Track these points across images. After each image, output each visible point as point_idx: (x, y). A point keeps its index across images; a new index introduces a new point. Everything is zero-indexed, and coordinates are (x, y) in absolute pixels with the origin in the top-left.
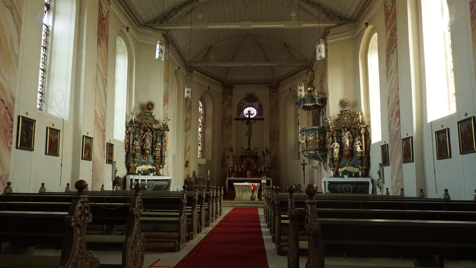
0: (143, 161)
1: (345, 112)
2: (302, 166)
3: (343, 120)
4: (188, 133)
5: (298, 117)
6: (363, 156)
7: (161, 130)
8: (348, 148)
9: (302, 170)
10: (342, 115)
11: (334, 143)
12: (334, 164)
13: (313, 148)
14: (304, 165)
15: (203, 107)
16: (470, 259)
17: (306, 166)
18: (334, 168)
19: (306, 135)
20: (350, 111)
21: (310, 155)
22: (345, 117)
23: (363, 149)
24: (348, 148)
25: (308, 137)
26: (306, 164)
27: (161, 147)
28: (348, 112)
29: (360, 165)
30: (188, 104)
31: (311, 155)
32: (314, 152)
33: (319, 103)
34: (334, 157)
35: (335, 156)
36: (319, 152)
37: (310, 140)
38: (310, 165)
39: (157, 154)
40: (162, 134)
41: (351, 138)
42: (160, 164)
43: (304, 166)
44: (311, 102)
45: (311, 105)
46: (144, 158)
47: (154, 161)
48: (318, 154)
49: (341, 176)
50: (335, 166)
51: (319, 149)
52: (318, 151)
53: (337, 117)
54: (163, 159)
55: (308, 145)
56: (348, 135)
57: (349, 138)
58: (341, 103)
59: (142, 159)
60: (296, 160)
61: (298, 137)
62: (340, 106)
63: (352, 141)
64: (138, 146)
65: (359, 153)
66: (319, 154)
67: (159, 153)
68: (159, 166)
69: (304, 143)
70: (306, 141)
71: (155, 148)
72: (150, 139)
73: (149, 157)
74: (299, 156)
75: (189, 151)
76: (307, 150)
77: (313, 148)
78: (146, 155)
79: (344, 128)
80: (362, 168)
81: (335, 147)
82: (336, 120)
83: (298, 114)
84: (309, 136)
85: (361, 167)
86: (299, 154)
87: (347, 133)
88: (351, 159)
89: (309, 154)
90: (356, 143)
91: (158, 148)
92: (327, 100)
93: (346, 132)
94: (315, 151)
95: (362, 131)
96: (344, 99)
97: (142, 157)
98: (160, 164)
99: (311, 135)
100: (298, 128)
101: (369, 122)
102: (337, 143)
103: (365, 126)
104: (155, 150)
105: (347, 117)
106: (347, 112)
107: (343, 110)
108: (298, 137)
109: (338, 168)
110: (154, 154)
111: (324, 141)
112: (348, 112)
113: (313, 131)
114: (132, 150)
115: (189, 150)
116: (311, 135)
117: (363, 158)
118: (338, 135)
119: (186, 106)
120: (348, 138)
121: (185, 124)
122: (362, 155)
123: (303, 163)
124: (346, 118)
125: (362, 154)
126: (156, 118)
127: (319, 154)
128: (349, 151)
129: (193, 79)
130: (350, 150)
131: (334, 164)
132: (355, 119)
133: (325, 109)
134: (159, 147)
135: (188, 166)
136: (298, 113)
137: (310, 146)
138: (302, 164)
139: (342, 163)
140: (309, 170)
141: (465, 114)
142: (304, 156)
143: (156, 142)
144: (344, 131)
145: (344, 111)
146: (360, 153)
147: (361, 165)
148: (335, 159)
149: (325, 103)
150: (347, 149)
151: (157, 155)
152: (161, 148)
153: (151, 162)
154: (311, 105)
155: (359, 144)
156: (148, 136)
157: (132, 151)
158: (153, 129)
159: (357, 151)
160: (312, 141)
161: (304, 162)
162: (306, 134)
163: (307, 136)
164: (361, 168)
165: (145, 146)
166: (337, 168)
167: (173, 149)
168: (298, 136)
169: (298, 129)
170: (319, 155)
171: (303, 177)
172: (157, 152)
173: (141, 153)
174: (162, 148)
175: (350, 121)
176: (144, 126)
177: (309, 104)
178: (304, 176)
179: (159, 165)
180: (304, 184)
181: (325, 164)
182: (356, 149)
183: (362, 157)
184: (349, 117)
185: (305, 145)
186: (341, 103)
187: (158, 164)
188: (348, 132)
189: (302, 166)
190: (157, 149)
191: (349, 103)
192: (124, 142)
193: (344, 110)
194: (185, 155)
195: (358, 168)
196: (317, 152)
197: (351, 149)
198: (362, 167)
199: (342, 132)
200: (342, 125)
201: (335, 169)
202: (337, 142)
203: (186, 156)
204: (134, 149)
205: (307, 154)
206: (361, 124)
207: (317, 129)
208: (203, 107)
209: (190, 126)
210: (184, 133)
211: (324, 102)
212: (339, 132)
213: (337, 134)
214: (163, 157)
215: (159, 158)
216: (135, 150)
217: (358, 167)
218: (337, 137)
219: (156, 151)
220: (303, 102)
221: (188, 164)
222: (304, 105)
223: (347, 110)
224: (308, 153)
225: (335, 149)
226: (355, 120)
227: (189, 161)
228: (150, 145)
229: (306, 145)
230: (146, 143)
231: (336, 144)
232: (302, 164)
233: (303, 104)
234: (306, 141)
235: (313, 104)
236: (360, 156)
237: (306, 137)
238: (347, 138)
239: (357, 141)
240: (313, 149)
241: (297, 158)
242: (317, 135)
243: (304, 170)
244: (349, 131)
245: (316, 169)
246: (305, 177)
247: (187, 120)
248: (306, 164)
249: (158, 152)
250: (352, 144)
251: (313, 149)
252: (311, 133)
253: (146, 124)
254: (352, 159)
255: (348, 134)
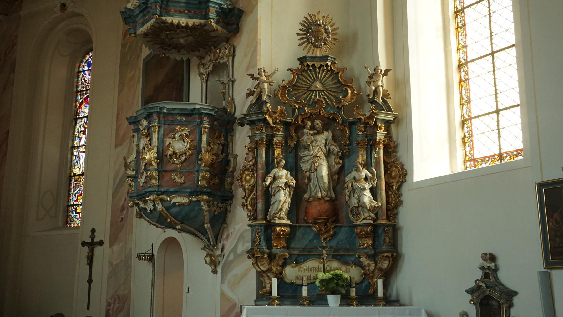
1: (317, 65)
2: (86, 249)
3: (308, 89)
5: (74, 99)
6: (379, 222)
8: (324, 193)
9: (85, 261)
10: (304, 73)
11: (275, 170)
12: (270, 247)
13: (185, 185)
14: (92, 245)
17: (98, 250)
18: (270, 263)
19: (158, 132)
20: (333, 63)
21: (168, 209)
22: (314, 81)
23: (382, 199)
24: (324, 193)
25: (168, 141)
26: (101, 243)
28: (327, 66)
29: (369, 257)
31: (174, 210)
32: (186, 200)
33: (217, 23)
34: (277, 221)
35: (280, 218)
36: (208, 202)
37: (174, 153)
38: (116, 248)
41: (333, 157)
43: (92, 251)
44: (190, 12)
45: (190, 25)
48: (201, 210)
49: (305, 299)
50: (275, 256)
51: (209, 190)
52: (205, 197)
53: (289, 77)
55: (166, 171)
56: (325, 146)
57: (328, 155)
58: (307, 31)
60: (58, 228)
61: (69, 159)
62: (300, 39)
63: (336, 167)
65: (369, 210)
66: (205, 207)
69: (153, 163)
70: (158, 152)
74: (68, 216)
76: (163, 190)
77: (185, 185)
79: (311, 117)
80: (372, 267)
81: (283, 185)
82: (284, 87)
83: (77, 92)
84: (170, 135)
85: (368, 262)
86: (68, 211)
87: (322, 138)
88: (332, 233)
89: (166, 204)
90: (354, 174)
92: (243, 18)
93: (318, 133)
94: (191, 194)
95: (381, 135)
96: (321, 17)
99: (179, 134)
100: (71, 132)
101: (405, 103)
102: (285, 172)
103: (391, 118)
105: (321, 82)
106: (324, 64)
107: (310, 54)
108: (69, 159)
109: (284, 265)
111: (222, 161)
112: (329, 64)
113: (190, 119)
116: (179, 134)
117: (380, 231)
118: (286, 143)
120: (326, 156)
122: (374, 221)
123: (89, 240)
124: (318, 85)
125: (376, 215)
127: (205, 207)
128: (328, 201)
130: (332, 201)
131: (270, 247)
132: (352, 93)
133: (232, 49)
136: (77, 86)
137: (174, 176)
138: (84, 244)
139: (298, 246)
140: (111, 263)
142: (243, 196)
144: (312, 128)
145: (315, 57)
146: (372, 212)
147: (373, 257)
148: (278, 228)
149: (235, 26)
150: (320, 195)
154: (190, 25)
155: (366, 179)
159: (361, 205)
160: (183, 158)
161: (93, 237)
162: (159, 127)
163: (164, 136)
164: (369, 265)
166: (281, 263)
168: (69, 156)
169: (71, 134)
170: (206, 213)
171: (87, 284)
175: (332, 98)
177: (182, 17)
178: (90, 281)
180: (88, 309)
181: (217, 249)
182: (359, 197)
183: (375, 227)
184: (330, 83)
185: (155, 170)
186: (307, 31)
188: (326, 133)
189: (86, 249)
191: (336, 34)
193: (314, 55)
195: (359, 268)
196: (199, 201)
197: (333, 196)
198: (376, 264)
199: (306, 131)
200: (304, 106)
201: (274, 269)
202: (285, 167)
205: (160, 207)
206: (379, 107)
207: (206, 114)
211: (233, 24)
212: (292, 131)
213: (287, 137)
217: (359, 264)
218: (285, 147)
220: (161, 8)
222: (164, 18)
223: (326, 58)
224: (161, 200)
225: (282, 192)
226: (349, 95)
229: (159, 171)
231: (284, 175)
232: (84, 244)
233: (161, 15)
234: (161, 157)
235: (197, 21)
236: (372, 222)
237: (161, 141)
238: (323, 157)
239: (361, 167)
240: (186, 188)
241: (60, 223)
242: (205, 137)
243: (90, 264)
244: (327, 130)
245: (146, 266)
246: (92, 285)
248: (101, 243)
250: (336, 177)
251: (186, 188)
252: (182, 125)
254: (335, 234)
255: (326, 140)
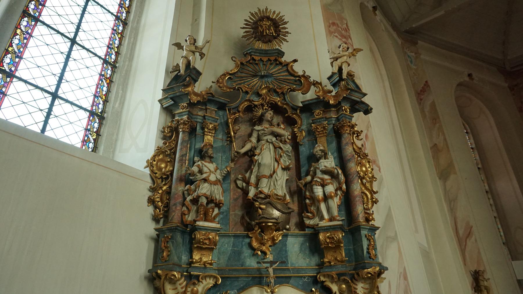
0: (252, 263)
4: (449, 183)
7: (326, 106)
15: (469, 131)
16: (157, 214)
27: (342, 177)
30: (427, 109)
39: (322, 218)
40: (338, 119)
42: (353, 278)
46: (255, 244)
47: (314, 261)
54: (365, 243)
59: (247, 252)
64: (212, 183)
67: (335, 212)
68: (349, 287)
71: (312, 191)
72: (275, 148)
73: (284, 243)
75: (473, 239)
78: (264, 229)
91: (323, 186)
97: (247, 240)
98: (353, 278)
104: (314, 200)
110: (311, 222)
114: (184, 208)
115: (469, 234)
119: (422, 111)
121: (433, 158)
126: (298, 68)
129: (422, 57)
134: (326, 177)
135: (487, 288)
141: (477, 270)
143: (314, 159)
151: (323, 224)
152: (340, 183)
153: (298, 270)
156: (270, 138)
157: (183, 214)
158: (289, 111)
165: (257, 186)
167: (417, 231)
172: (323, 206)
173: (242, 224)
174: (348, 182)
176: (249, 100)
179: (345, 282)
187: (339, 275)
190: (319, 191)
192: (148, 171)
194: (463, 251)
203: (467, 254)
204: (189, 198)
208: (469, 131)
209: (451, 165)
210: (439, 183)
214: (364, 232)
215: (339, 241)
216: (195, 201)
219: (319, 201)
221: (482, 283)
227: (482, 269)
228: (282, 177)
230: (259, 164)
247: (435, 150)
249: (328, 209)
253: (259, 95)
